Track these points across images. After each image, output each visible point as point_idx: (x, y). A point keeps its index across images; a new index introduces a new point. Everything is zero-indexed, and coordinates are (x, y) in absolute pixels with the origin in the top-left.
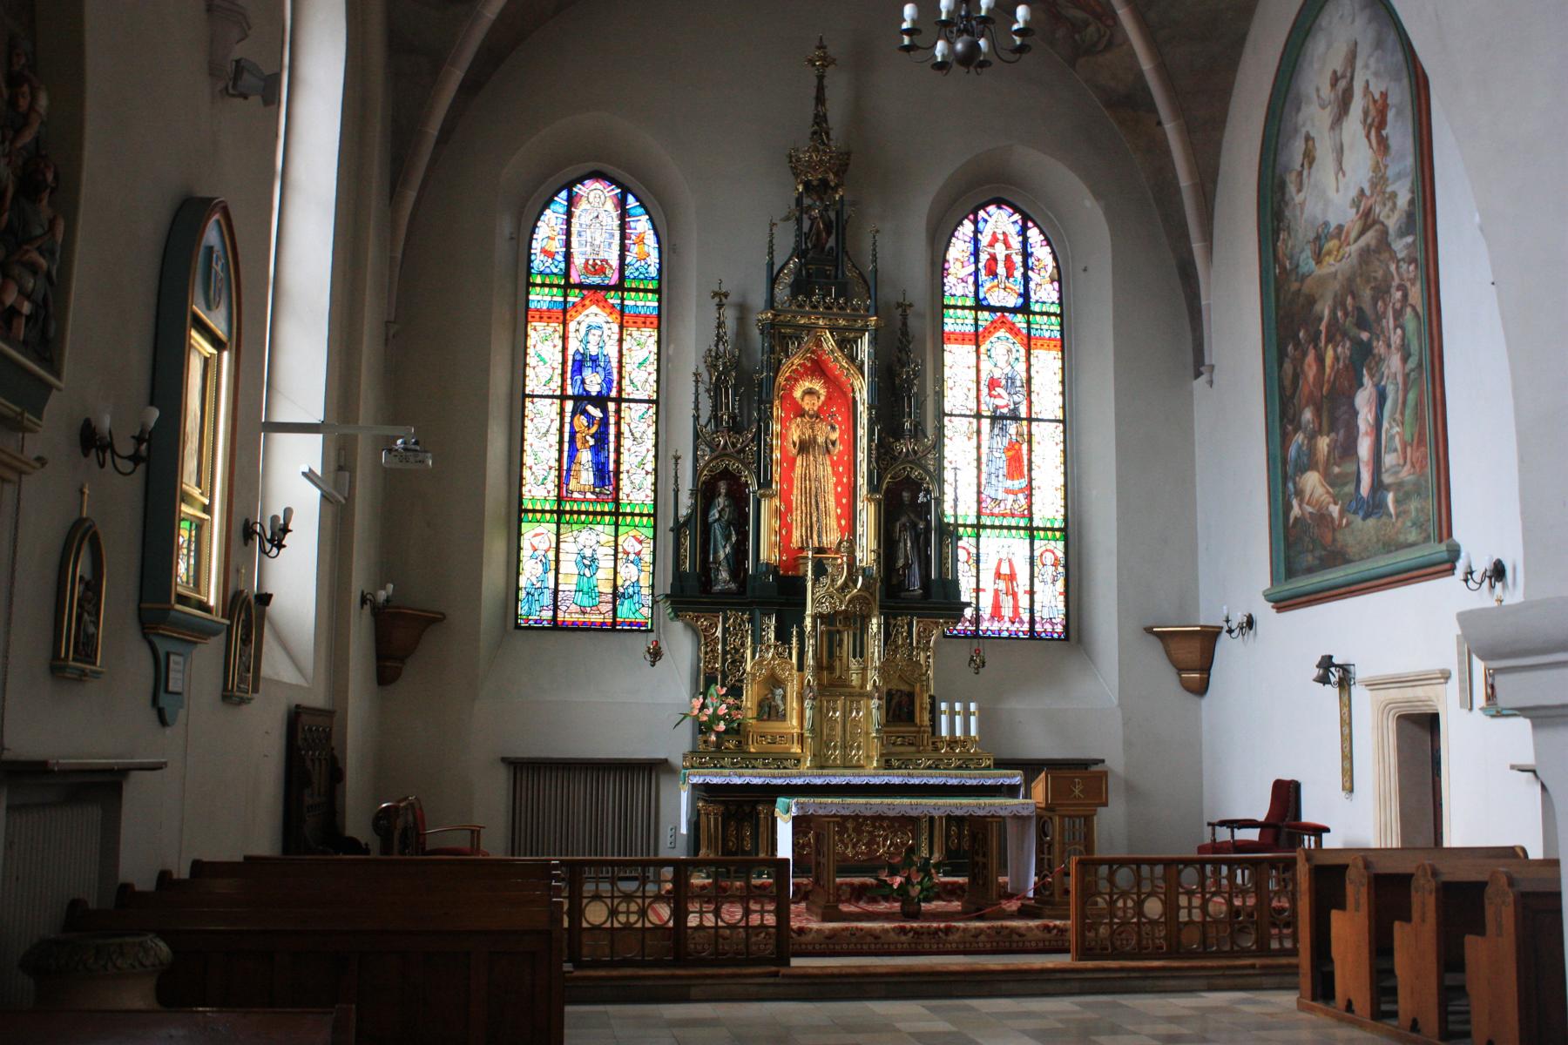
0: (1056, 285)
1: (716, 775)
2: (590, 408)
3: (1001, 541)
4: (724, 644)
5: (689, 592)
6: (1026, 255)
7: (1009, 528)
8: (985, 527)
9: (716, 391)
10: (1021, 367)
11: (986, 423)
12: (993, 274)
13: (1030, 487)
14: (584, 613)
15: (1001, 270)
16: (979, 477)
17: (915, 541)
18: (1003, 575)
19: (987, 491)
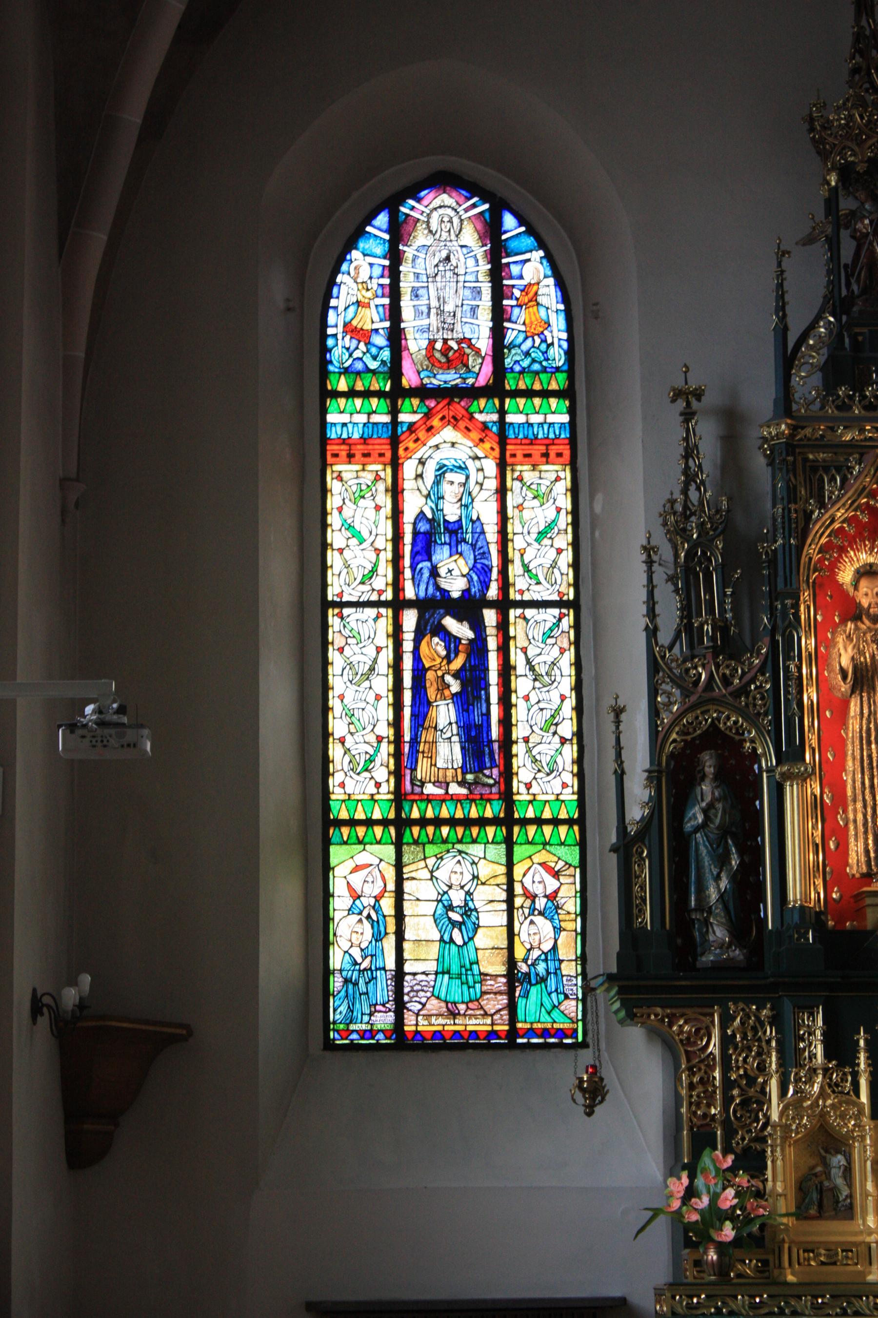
2: (450, 623)
4: (726, 1068)
5: (655, 964)
9: (688, 577)
14: (453, 1014)
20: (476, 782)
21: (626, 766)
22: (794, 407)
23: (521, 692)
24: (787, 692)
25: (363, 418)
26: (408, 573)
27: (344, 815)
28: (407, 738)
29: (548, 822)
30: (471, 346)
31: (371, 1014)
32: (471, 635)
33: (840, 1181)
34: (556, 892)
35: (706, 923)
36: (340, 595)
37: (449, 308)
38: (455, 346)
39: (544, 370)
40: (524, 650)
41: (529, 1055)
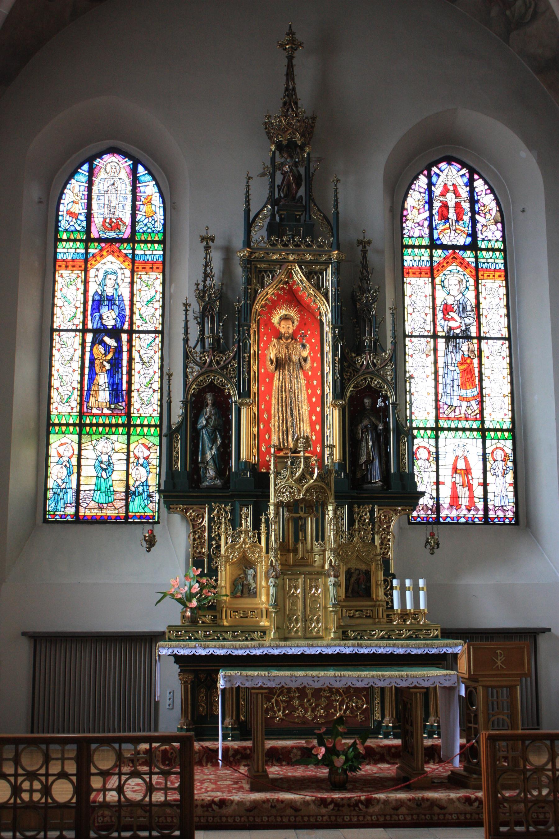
0: (499, 226)
1: (183, 647)
2: (107, 339)
3: (457, 441)
4: (210, 532)
5: (181, 487)
6: (473, 201)
7: (464, 430)
8: (443, 429)
10: (471, 294)
11: (441, 342)
12: (446, 219)
13: (481, 394)
14: (101, 509)
15: (452, 215)
16: (436, 387)
17: (376, 441)
18: (454, 467)
19: (444, 399)
20: (115, 408)
21: (172, 399)
22: (252, 244)
23: (137, 370)
24: (243, 368)
25: (73, 251)
26: (89, 317)
27: (57, 421)
28: (86, 388)
29: (146, 426)
30: (122, 221)
31: (65, 508)
32: (116, 345)
33: (251, 581)
34: (148, 456)
35: (206, 468)
36: (60, 326)
37: (113, 205)
38: (115, 221)
39: (153, 232)
40: (139, 352)
41: (133, 527)
